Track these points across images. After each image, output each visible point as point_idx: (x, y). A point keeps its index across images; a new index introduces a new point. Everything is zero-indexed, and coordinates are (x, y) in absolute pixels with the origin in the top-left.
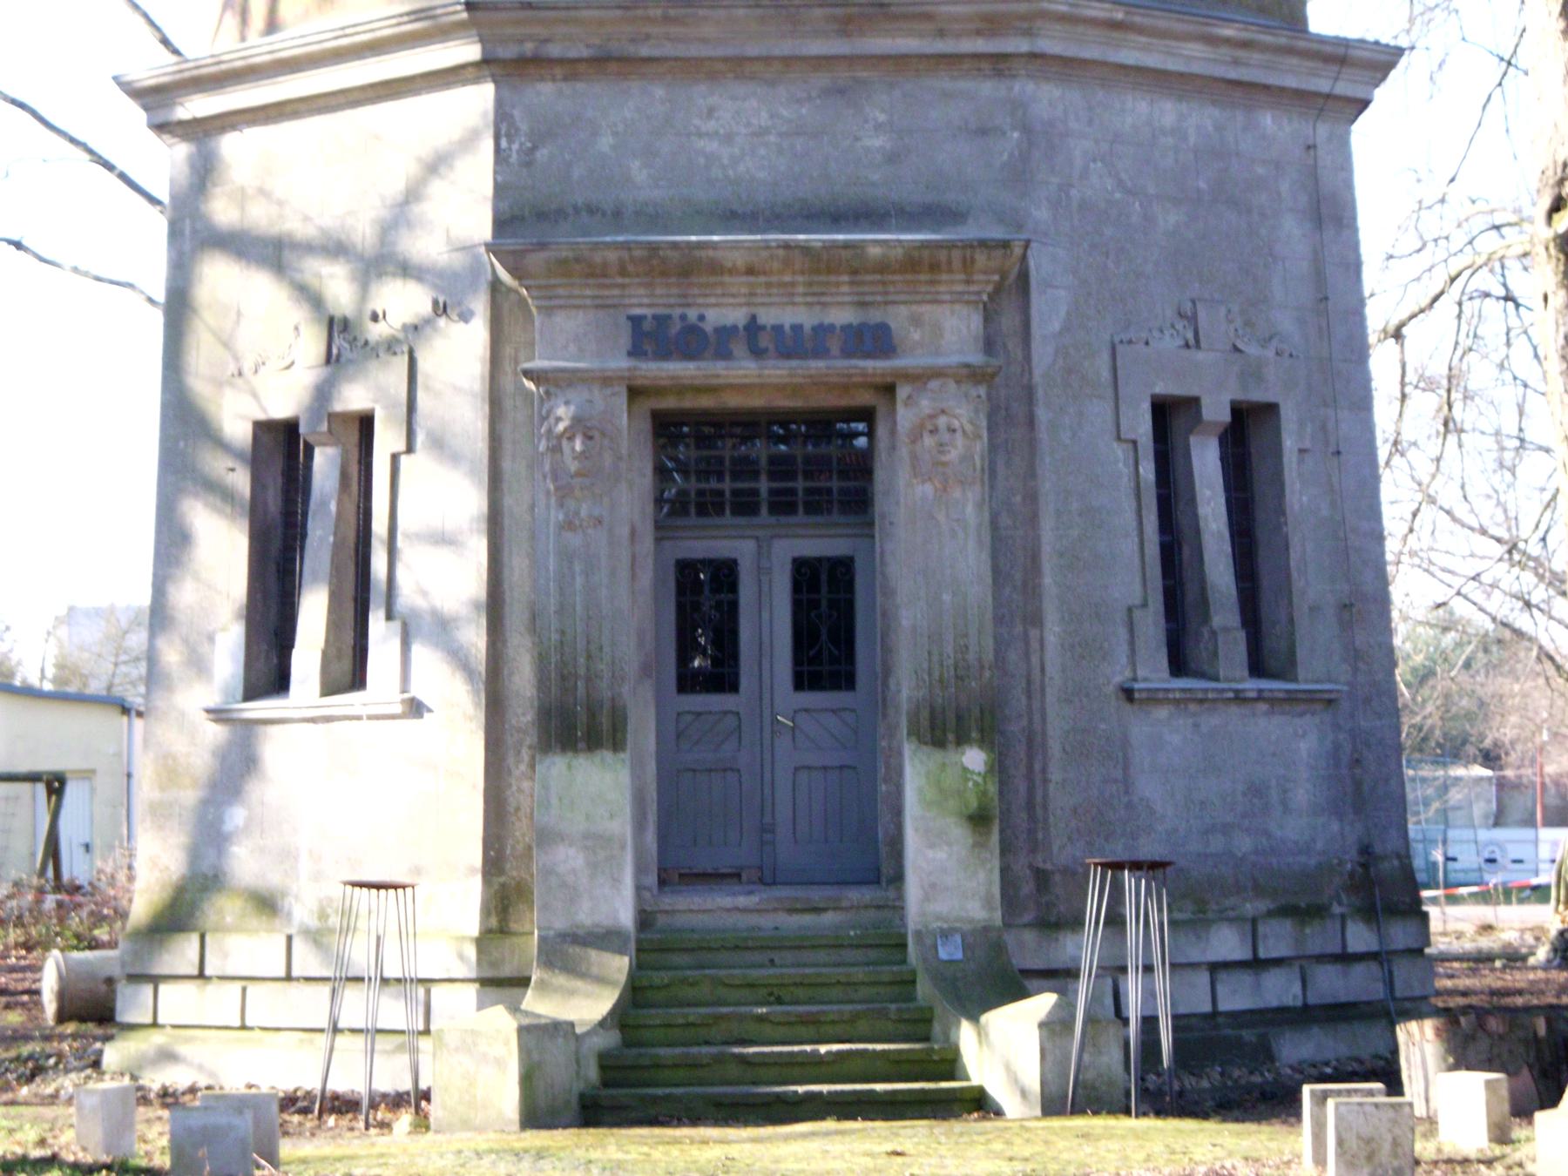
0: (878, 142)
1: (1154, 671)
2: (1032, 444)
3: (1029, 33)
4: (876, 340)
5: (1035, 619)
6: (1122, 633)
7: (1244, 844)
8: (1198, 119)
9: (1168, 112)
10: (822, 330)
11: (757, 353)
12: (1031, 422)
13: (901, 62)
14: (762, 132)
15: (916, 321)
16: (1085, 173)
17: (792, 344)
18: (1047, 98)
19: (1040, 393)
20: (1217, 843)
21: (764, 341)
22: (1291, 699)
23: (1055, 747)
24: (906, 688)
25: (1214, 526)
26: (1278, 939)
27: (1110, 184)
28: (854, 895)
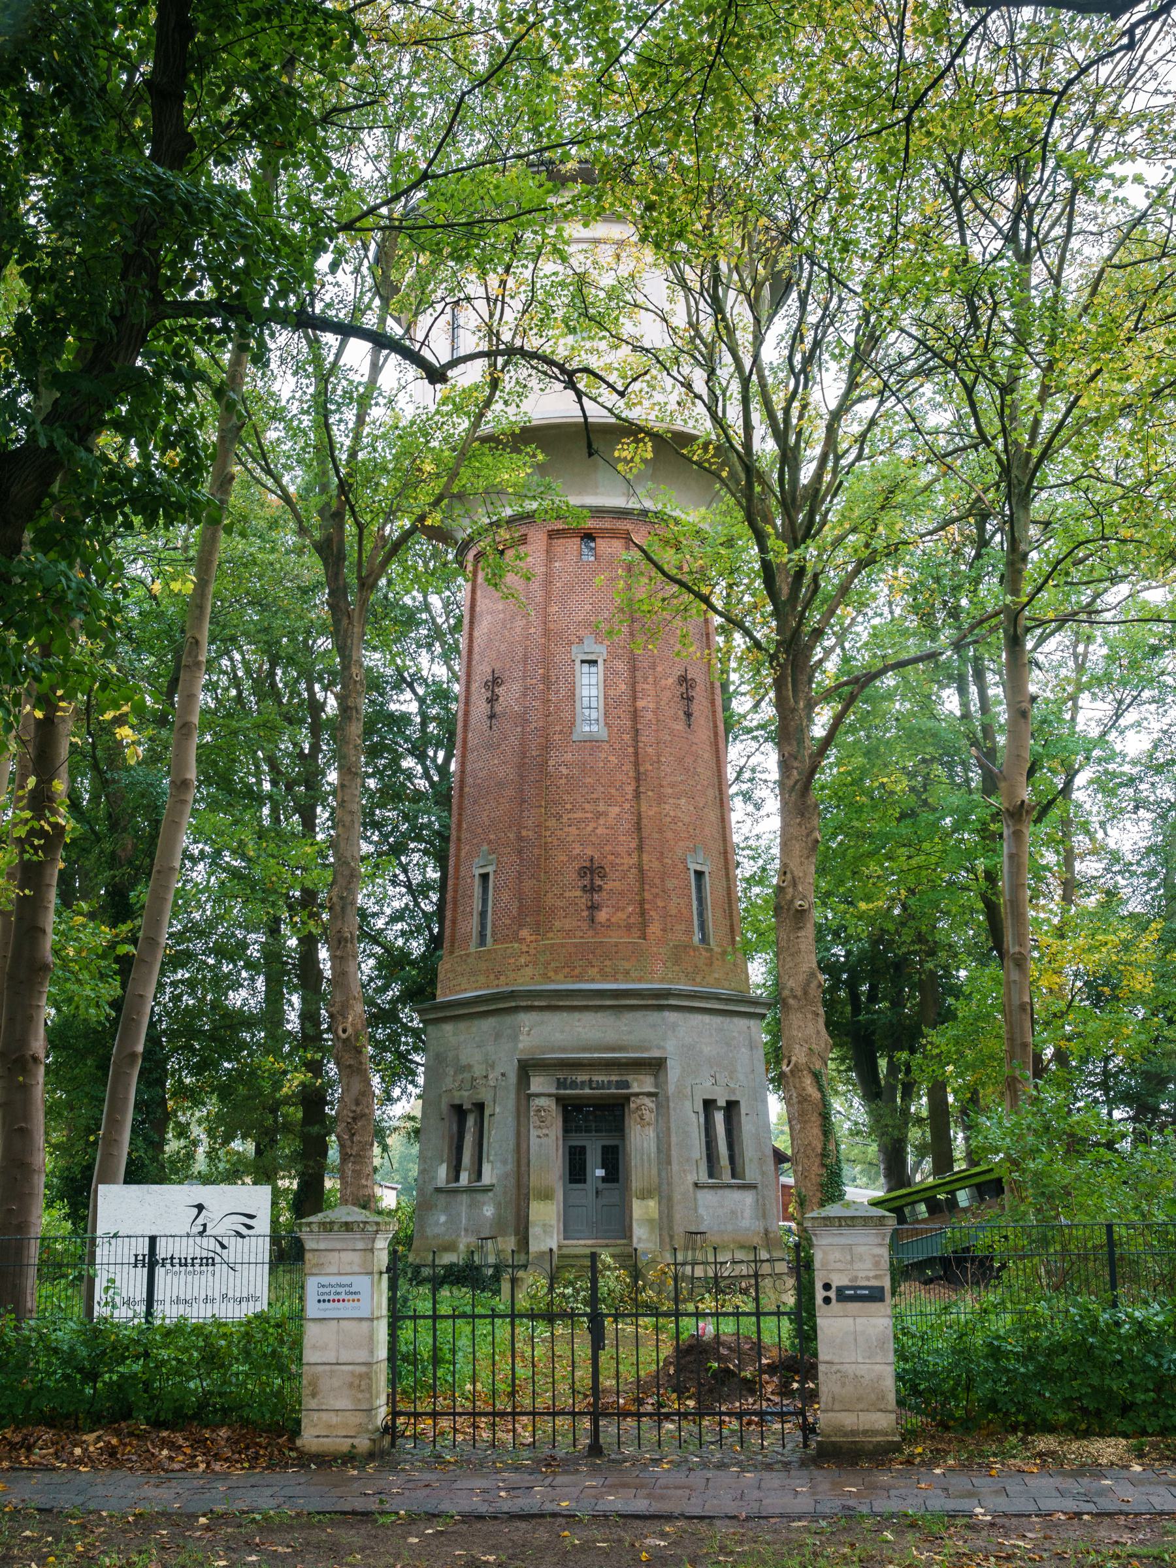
5: (669, 1163)
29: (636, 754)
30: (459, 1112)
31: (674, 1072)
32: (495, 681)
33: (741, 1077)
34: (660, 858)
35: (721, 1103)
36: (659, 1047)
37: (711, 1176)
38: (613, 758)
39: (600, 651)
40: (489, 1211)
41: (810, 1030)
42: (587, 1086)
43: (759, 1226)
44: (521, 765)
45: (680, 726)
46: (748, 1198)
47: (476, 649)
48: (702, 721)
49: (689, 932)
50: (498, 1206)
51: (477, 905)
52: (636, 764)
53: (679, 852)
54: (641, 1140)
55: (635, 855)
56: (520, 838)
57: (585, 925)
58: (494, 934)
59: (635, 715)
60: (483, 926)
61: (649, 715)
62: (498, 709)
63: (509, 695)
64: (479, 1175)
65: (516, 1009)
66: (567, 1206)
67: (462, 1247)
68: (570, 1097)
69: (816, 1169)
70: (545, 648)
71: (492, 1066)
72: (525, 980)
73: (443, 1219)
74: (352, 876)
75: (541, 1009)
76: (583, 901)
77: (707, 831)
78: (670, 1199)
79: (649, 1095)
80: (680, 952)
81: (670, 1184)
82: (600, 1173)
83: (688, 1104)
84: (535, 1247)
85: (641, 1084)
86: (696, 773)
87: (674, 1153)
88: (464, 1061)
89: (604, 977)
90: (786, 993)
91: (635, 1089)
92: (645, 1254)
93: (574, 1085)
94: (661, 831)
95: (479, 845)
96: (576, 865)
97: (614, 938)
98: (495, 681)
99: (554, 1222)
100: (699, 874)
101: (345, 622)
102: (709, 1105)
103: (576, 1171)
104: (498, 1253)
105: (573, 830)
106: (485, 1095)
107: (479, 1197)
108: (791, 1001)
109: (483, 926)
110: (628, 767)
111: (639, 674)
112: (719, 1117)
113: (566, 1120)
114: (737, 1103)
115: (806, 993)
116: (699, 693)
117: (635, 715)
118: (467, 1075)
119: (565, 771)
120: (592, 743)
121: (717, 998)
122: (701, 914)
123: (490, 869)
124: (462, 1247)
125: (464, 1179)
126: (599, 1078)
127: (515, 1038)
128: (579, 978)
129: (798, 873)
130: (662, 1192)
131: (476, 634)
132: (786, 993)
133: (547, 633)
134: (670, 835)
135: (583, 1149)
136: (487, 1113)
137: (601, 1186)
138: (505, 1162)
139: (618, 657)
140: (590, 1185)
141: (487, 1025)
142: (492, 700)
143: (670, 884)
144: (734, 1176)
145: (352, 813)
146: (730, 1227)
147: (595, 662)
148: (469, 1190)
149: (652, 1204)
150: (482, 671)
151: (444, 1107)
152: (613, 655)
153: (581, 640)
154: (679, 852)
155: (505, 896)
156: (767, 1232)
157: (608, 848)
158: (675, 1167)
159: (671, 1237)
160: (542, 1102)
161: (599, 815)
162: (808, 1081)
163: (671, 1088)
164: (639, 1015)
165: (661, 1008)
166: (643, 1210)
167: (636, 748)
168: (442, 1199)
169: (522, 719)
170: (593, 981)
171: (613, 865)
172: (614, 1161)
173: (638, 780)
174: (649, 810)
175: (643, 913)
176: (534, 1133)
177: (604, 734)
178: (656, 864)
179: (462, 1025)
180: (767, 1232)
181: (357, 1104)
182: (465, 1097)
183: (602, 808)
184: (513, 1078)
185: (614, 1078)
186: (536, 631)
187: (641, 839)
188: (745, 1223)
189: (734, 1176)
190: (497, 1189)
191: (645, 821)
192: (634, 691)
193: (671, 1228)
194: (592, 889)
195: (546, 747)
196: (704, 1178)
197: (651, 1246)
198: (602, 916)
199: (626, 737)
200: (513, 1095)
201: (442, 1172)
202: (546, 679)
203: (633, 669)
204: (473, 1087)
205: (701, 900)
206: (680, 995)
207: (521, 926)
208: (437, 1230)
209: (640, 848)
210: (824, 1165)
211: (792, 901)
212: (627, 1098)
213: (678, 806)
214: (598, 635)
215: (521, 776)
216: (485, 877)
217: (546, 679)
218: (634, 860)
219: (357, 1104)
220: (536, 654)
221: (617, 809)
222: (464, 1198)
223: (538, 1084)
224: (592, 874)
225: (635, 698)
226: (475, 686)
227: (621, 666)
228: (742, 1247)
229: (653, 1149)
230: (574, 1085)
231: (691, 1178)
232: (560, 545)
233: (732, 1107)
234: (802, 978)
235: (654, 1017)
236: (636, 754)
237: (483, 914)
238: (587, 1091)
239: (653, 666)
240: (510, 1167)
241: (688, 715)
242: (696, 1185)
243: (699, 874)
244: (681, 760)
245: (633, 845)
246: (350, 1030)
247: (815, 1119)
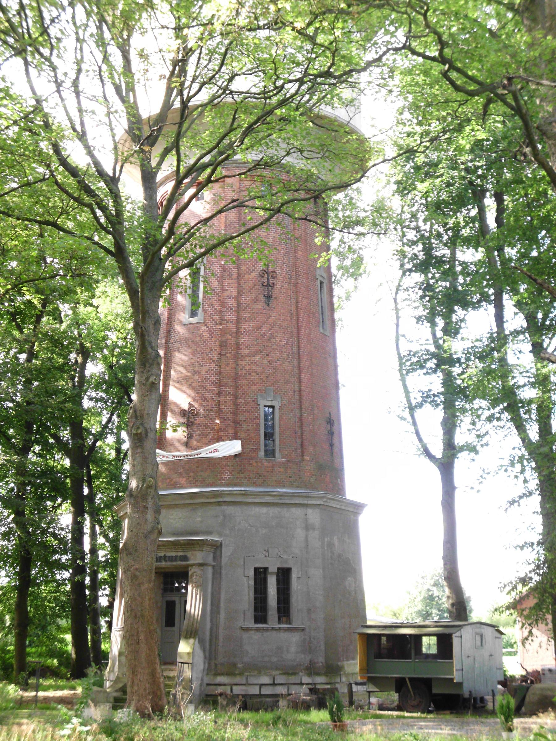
0: (199, 519)
1: (251, 624)
2: (221, 577)
3: (221, 497)
4: (185, 558)
5: (219, 613)
6: (242, 615)
7: (274, 659)
8: (275, 511)
9: (264, 510)
10: (176, 556)
11: (166, 561)
12: (221, 573)
13: (202, 503)
14: (180, 518)
15: (192, 554)
16: (240, 523)
17: (171, 559)
18: (229, 510)
19: (223, 568)
20: (267, 659)
21: (167, 559)
22: (289, 630)
23: (221, 638)
24: (184, 627)
25: (272, 593)
26: (280, 679)
27: (247, 525)
28: (255, 691)
45: (260, 306)
87: (222, 605)
163: (224, 560)
170: (182, 487)
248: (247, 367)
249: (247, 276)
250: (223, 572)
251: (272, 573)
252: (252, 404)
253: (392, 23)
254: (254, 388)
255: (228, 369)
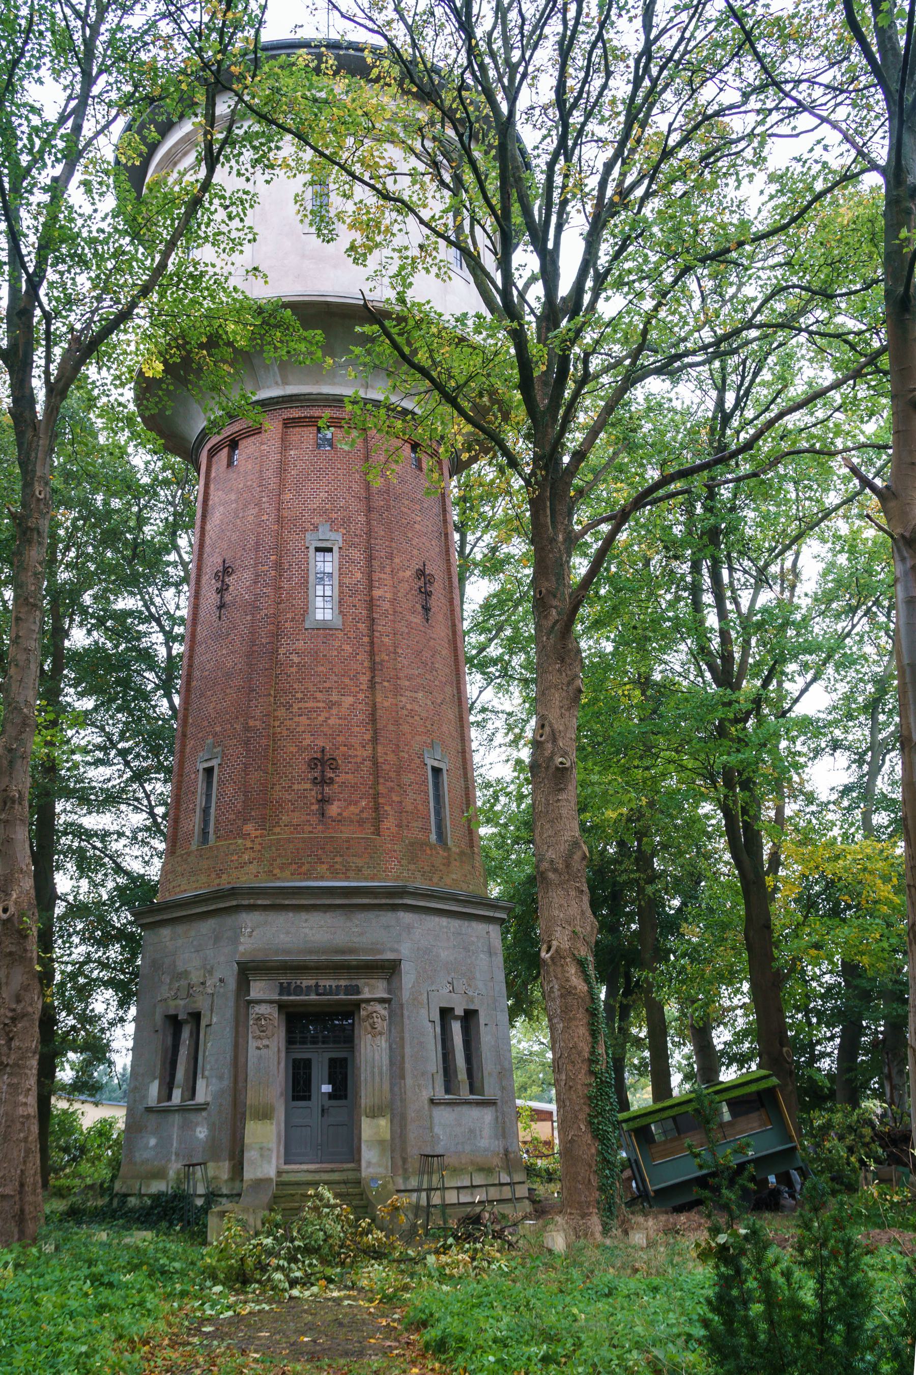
5: (403, 1077)
29: (372, 643)
30: (174, 1023)
31: (408, 976)
32: (226, 570)
33: (480, 985)
34: (396, 751)
35: (459, 1012)
36: (393, 950)
37: (447, 1091)
38: (347, 647)
39: (336, 539)
40: (202, 1133)
41: (574, 910)
42: (314, 991)
43: (497, 1145)
44: (250, 654)
45: (417, 619)
46: (487, 1116)
47: (208, 541)
48: (440, 618)
49: (426, 830)
50: (212, 1127)
51: (200, 800)
52: (372, 654)
53: (416, 747)
54: (372, 1051)
55: (369, 748)
56: (247, 729)
57: (314, 820)
58: (217, 830)
59: (371, 604)
60: (206, 822)
61: (386, 605)
62: (228, 598)
63: (240, 584)
64: (192, 1092)
65: (238, 908)
66: (289, 1125)
67: (172, 1174)
68: (294, 1004)
69: (583, 1077)
70: (279, 535)
71: (211, 972)
72: (248, 876)
73: (153, 1142)
74: (24, 724)
75: (265, 908)
76: (314, 794)
77: (445, 728)
78: (403, 1117)
79: (382, 1001)
80: (416, 849)
81: (403, 1101)
82: (326, 1088)
83: (424, 1012)
84: (249, 1174)
85: (372, 988)
86: (433, 669)
87: (408, 1066)
88: (180, 968)
89: (335, 875)
90: (545, 865)
91: (366, 994)
92: (374, 1179)
93: (298, 990)
94: (397, 723)
95: (203, 739)
96: (306, 756)
97: (346, 832)
98: (226, 570)
99: (273, 1145)
100: (437, 771)
101: (29, 434)
102: (446, 1013)
103: (299, 1086)
104: (208, 1182)
105: (303, 720)
106: (202, 1004)
107: (193, 1117)
108: (551, 875)
109: (206, 822)
110: (363, 657)
111: (375, 563)
112: (456, 1027)
113: (290, 1031)
114: (475, 1012)
115: (568, 866)
116: (437, 589)
117: (371, 604)
118: (183, 983)
119: (296, 659)
120: (325, 629)
121: (454, 898)
122: (438, 813)
123: (214, 763)
124: (172, 1174)
125: (177, 1096)
126: (327, 982)
127: (235, 941)
128: (307, 876)
129: (559, 726)
130: (394, 1109)
131: (208, 527)
132: (545, 865)
133: (280, 520)
134: (406, 728)
135: (307, 1063)
136: (203, 1023)
137: (328, 1103)
138: (221, 1078)
139: (354, 545)
140: (315, 1103)
141: (207, 927)
142: (221, 591)
143: (408, 778)
144: (472, 1092)
145: (27, 650)
146: (468, 1148)
147: (330, 550)
148: (182, 1109)
149: (383, 1123)
150: (213, 562)
151: (159, 1018)
152: (349, 543)
153: (316, 528)
154: (416, 747)
155: (230, 790)
156: (507, 1153)
157: (341, 739)
158: (409, 1081)
159: (404, 1160)
160: (263, 1009)
161: (331, 705)
162: (572, 970)
163: (406, 995)
164: (371, 915)
165: (394, 908)
166: (374, 1130)
167: (372, 637)
168: (153, 1118)
169: (254, 607)
170: (322, 878)
171: (346, 757)
172: (342, 1076)
173: (373, 669)
174: (384, 702)
175: (377, 808)
176: (252, 1044)
177: (338, 623)
178: (391, 757)
179: (180, 929)
180: (507, 1153)
181: (18, 1001)
182: (180, 1007)
183: (334, 698)
184: (232, 983)
185: (343, 983)
186: (269, 518)
187: (375, 731)
188: (484, 1143)
189: (472, 1092)
190: (212, 1107)
191: (379, 712)
192: (371, 581)
193: (404, 1149)
194: (322, 782)
195: (277, 635)
196: (440, 1094)
197: (381, 1170)
198: (334, 809)
199: (362, 626)
200: (231, 1003)
201: (154, 1089)
202: (278, 565)
203: (370, 558)
204: (189, 995)
205: (438, 798)
206: (415, 894)
207: (246, 821)
208: (146, 1155)
209: (375, 740)
210: (592, 1073)
211: (551, 759)
212: (357, 1005)
213: (415, 700)
214: (334, 525)
215: (249, 665)
216: (209, 771)
217: (278, 565)
218: (368, 752)
219: (18, 1001)
220: (269, 541)
221: (351, 699)
222: (177, 1119)
223: (258, 989)
224: (323, 766)
225: (371, 587)
226: (205, 579)
227: (357, 554)
228: (481, 1169)
229: (386, 1061)
230: (298, 990)
231: (426, 1094)
232: (296, 434)
233: (470, 1016)
234: (563, 847)
235: (388, 917)
236: (372, 643)
237: (206, 811)
238: (313, 997)
239: (391, 557)
240: (227, 1083)
241: (426, 609)
242: (432, 1101)
243: (437, 771)
244: (419, 653)
245: (368, 737)
246: (12, 909)
247: (581, 1015)
248: (409, 707)
249: (401, 574)
250: (406, 1013)
251: (456, 1018)
252: (418, 761)
253: (72, 220)
254: (418, 738)
255: (386, 704)
